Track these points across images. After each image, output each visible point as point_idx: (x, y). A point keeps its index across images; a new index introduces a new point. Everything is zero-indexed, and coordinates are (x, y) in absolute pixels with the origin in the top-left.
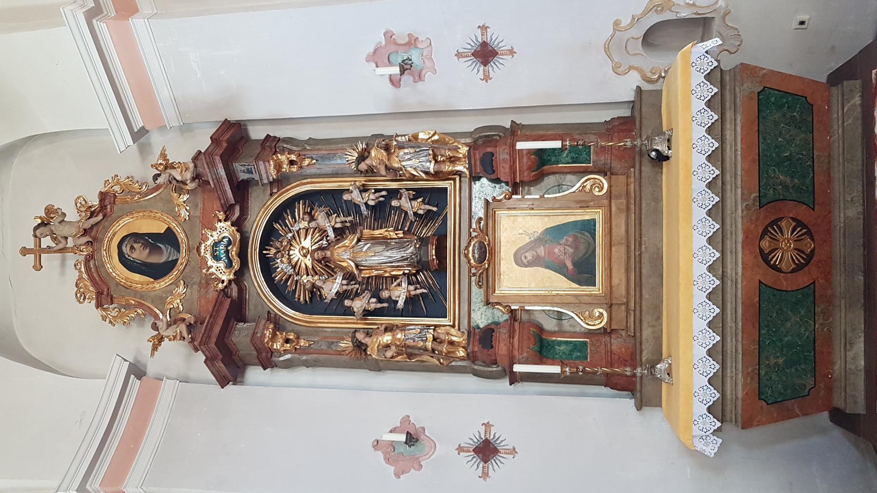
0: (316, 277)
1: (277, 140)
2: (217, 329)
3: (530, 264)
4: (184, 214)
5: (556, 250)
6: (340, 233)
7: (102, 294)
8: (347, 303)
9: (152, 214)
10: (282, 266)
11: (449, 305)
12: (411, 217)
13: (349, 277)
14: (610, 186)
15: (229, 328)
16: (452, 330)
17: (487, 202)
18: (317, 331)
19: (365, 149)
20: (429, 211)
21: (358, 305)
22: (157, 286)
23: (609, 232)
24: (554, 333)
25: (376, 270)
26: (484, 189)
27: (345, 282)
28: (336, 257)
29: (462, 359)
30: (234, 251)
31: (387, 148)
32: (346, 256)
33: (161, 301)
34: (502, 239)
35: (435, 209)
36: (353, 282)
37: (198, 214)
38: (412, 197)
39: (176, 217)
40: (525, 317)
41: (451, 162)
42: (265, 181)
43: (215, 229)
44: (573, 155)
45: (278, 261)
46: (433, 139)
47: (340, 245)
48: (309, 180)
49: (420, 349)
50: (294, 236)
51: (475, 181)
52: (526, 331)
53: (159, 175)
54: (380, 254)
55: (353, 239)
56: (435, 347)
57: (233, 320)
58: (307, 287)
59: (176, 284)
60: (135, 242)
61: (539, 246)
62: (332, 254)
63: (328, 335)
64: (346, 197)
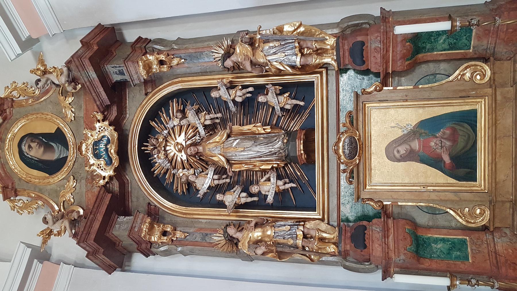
0: (192, 171)
1: (148, 41)
2: (96, 225)
3: (403, 159)
4: (70, 115)
5: (432, 144)
6: (211, 129)
7: (7, 188)
8: (219, 197)
9: (43, 116)
10: (160, 161)
11: (319, 198)
12: (279, 112)
13: (220, 171)
14: (493, 73)
15: (111, 222)
16: (322, 224)
17: (357, 95)
18: (194, 222)
19: (231, 46)
20: (296, 105)
21: (229, 199)
22: (52, 180)
23: (494, 123)
24: (429, 228)
25: (246, 164)
26: (350, 81)
27: (216, 177)
28: (207, 152)
29: (333, 255)
30: (112, 150)
31: (252, 43)
32: (216, 152)
33: (55, 194)
34: (372, 133)
35: (302, 103)
36: (225, 176)
37: (82, 114)
38: (278, 92)
39: (64, 118)
40: (396, 211)
41: (318, 54)
42: (137, 82)
43: (94, 129)
44: (451, 41)
45: (155, 156)
46: (299, 31)
47: (211, 141)
48: (180, 79)
49: (291, 246)
50: (169, 133)
51: (341, 73)
52: (400, 230)
53: (39, 80)
54: (251, 149)
55: (223, 135)
56: (305, 245)
57: (114, 213)
58: (183, 180)
59: (67, 179)
60: (32, 141)
61: (414, 139)
62: (204, 149)
63: (203, 226)
64: (214, 94)
